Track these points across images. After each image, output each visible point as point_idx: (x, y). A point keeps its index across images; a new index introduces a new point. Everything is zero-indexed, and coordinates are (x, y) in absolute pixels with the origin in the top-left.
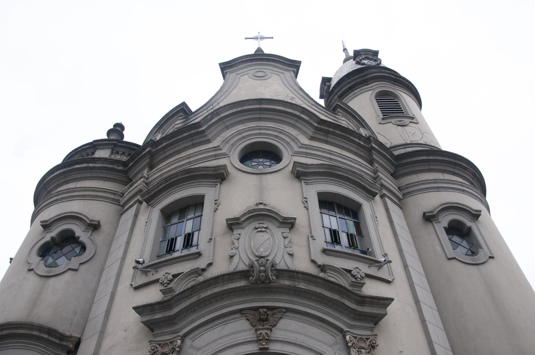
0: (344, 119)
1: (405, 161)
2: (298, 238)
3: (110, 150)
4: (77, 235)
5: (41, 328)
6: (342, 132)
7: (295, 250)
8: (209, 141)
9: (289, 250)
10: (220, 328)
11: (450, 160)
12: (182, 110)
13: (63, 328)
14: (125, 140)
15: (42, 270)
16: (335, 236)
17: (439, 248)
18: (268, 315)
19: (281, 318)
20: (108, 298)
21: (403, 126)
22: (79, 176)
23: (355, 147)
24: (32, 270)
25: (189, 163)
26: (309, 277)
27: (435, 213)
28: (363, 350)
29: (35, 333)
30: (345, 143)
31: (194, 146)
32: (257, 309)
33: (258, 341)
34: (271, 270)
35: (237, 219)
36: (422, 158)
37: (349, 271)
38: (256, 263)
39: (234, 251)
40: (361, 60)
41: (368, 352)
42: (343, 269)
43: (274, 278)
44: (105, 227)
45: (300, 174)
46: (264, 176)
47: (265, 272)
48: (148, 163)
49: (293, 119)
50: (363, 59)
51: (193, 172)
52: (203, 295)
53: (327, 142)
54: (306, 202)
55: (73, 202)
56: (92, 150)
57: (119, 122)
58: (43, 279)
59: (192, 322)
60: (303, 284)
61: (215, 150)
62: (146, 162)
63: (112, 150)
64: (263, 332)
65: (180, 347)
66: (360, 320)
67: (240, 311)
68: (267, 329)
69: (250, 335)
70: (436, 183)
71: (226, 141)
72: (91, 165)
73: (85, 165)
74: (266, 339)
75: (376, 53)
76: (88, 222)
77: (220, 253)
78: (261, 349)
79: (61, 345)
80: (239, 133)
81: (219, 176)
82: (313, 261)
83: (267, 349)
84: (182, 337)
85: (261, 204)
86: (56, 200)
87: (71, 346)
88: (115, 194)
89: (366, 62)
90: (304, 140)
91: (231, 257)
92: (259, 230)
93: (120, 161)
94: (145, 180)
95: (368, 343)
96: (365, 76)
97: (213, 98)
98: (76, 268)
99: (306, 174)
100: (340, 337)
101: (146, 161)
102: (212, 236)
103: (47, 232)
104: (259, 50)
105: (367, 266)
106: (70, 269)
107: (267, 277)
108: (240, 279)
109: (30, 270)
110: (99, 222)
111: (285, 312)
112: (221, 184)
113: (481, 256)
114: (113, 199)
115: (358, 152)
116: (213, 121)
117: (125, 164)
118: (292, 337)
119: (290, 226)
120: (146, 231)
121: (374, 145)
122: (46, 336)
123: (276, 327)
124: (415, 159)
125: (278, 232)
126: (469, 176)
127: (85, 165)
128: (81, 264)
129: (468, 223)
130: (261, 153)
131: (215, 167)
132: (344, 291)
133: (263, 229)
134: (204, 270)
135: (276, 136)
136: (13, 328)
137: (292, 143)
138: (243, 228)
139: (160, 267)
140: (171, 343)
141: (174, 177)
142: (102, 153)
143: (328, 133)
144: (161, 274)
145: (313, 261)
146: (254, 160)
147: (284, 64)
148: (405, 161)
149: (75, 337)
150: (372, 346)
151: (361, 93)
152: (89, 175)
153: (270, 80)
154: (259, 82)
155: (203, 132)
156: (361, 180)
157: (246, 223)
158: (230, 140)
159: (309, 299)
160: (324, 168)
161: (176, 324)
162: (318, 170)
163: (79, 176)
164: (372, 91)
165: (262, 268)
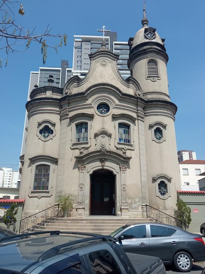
3: (51, 91)
4: (50, 127)
7: (111, 143)
9: (110, 143)
17: (151, 136)
27: (152, 125)
33: (102, 166)
37: (123, 148)
42: (121, 148)
45: (115, 117)
46: (104, 117)
64: (103, 164)
67: (98, 159)
76: (52, 123)
77: (94, 145)
80: (97, 98)
82: (115, 146)
85: (103, 128)
90: (117, 102)
91: (96, 145)
92: (103, 137)
99: (115, 118)
113: (162, 140)
121: (139, 100)
129: (162, 128)
130: (104, 107)
137: (113, 103)
145: (115, 146)
151: (143, 59)
155: (86, 96)
164: (147, 59)
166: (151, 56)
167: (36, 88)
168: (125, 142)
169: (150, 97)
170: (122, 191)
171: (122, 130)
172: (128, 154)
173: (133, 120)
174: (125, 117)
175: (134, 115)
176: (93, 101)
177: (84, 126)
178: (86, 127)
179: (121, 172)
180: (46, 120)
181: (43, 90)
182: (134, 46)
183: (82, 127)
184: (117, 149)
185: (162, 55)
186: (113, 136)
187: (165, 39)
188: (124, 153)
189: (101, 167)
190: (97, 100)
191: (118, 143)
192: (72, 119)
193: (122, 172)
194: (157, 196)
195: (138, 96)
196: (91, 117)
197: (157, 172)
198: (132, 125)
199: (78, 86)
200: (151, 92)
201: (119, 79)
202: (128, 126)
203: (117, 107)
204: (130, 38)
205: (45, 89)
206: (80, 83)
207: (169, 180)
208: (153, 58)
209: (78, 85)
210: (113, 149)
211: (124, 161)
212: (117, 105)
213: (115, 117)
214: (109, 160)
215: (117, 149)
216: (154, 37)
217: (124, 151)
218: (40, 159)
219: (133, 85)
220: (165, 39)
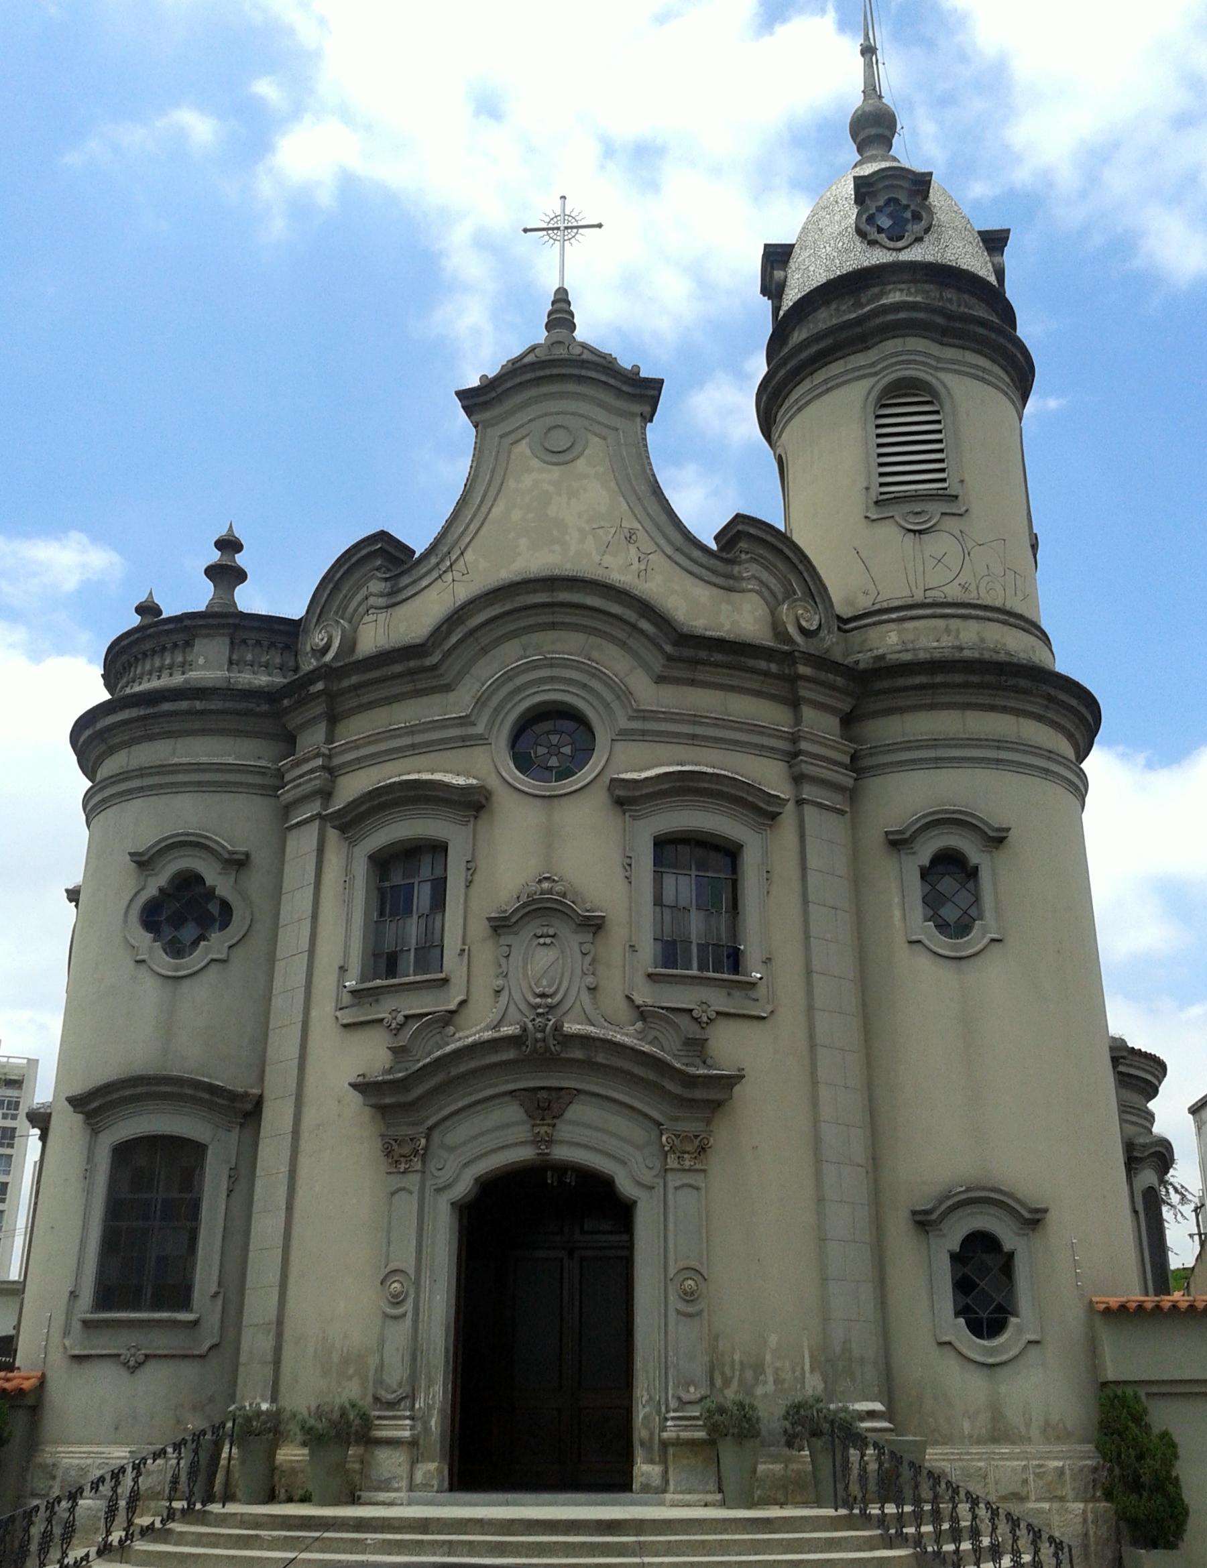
3: (227, 641)
20: (297, 1030)
24: (143, 961)
28: (686, 1156)
29: (189, 1091)
35: (505, 919)
38: (530, 1025)
39: (500, 982)
43: (558, 1048)
46: (556, 801)
47: (544, 1040)
54: (630, 865)
55: (180, 796)
58: (170, 981)
64: (543, 1130)
65: (426, 1148)
68: (549, 1125)
69: (522, 1132)
70: (935, 747)
77: (485, 993)
78: (539, 1154)
83: (547, 1154)
90: (647, 693)
91: (498, 992)
92: (542, 941)
98: (223, 956)
100: (656, 1132)
102: (464, 943)
103: (147, 876)
107: (547, 1049)
110: (247, 855)
112: (476, 818)
113: (976, 939)
114: (262, 786)
116: (454, 639)
120: (348, 903)
125: (573, 940)
128: (230, 947)
130: (550, 736)
133: (548, 940)
138: (516, 933)
140: (412, 1140)
143: (695, 663)
144: (382, 1011)
149: (254, 1095)
155: (434, 668)
164: (873, 380)
165: (539, 1035)
166: (903, 362)
167: (149, 620)
168: (700, 969)
169: (889, 641)
170: (672, 1314)
171: (680, 887)
173: (764, 811)
174: (164, 1097)
175: (770, 776)
176: (481, 702)
177: (426, 860)
178: (438, 873)
179: (671, 1185)
180: (188, 834)
181: (175, 637)
182: (792, 296)
183: (405, 882)
184: (642, 1014)
185: (983, 346)
186: (617, 934)
187: (1008, 231)
188: (697, 1047)
189: (524, 1154)
191: (650, 976)
192: (351, 821)
193: (674, 1180)
194: (946, 1339)
195: (799, 639)
196: (473, 804)
197: (937, 1157)
199: (394, 599)
200: (896, 603)
202: (731, 853)
203: (646, 728)
204: (766, 246)
205: (189, 628)
206: (405, 580)
207: (1034, 1221)
208: (907, 373)
209: (389, 594)
211: (693, 1098)
212: (643, 715)
213: (628, 799)
214: (582, 1097)
215: (642, 1014)
216: (918, 228)
217: (692, 1030)
219: (766, 568)
220: (1008, 231)
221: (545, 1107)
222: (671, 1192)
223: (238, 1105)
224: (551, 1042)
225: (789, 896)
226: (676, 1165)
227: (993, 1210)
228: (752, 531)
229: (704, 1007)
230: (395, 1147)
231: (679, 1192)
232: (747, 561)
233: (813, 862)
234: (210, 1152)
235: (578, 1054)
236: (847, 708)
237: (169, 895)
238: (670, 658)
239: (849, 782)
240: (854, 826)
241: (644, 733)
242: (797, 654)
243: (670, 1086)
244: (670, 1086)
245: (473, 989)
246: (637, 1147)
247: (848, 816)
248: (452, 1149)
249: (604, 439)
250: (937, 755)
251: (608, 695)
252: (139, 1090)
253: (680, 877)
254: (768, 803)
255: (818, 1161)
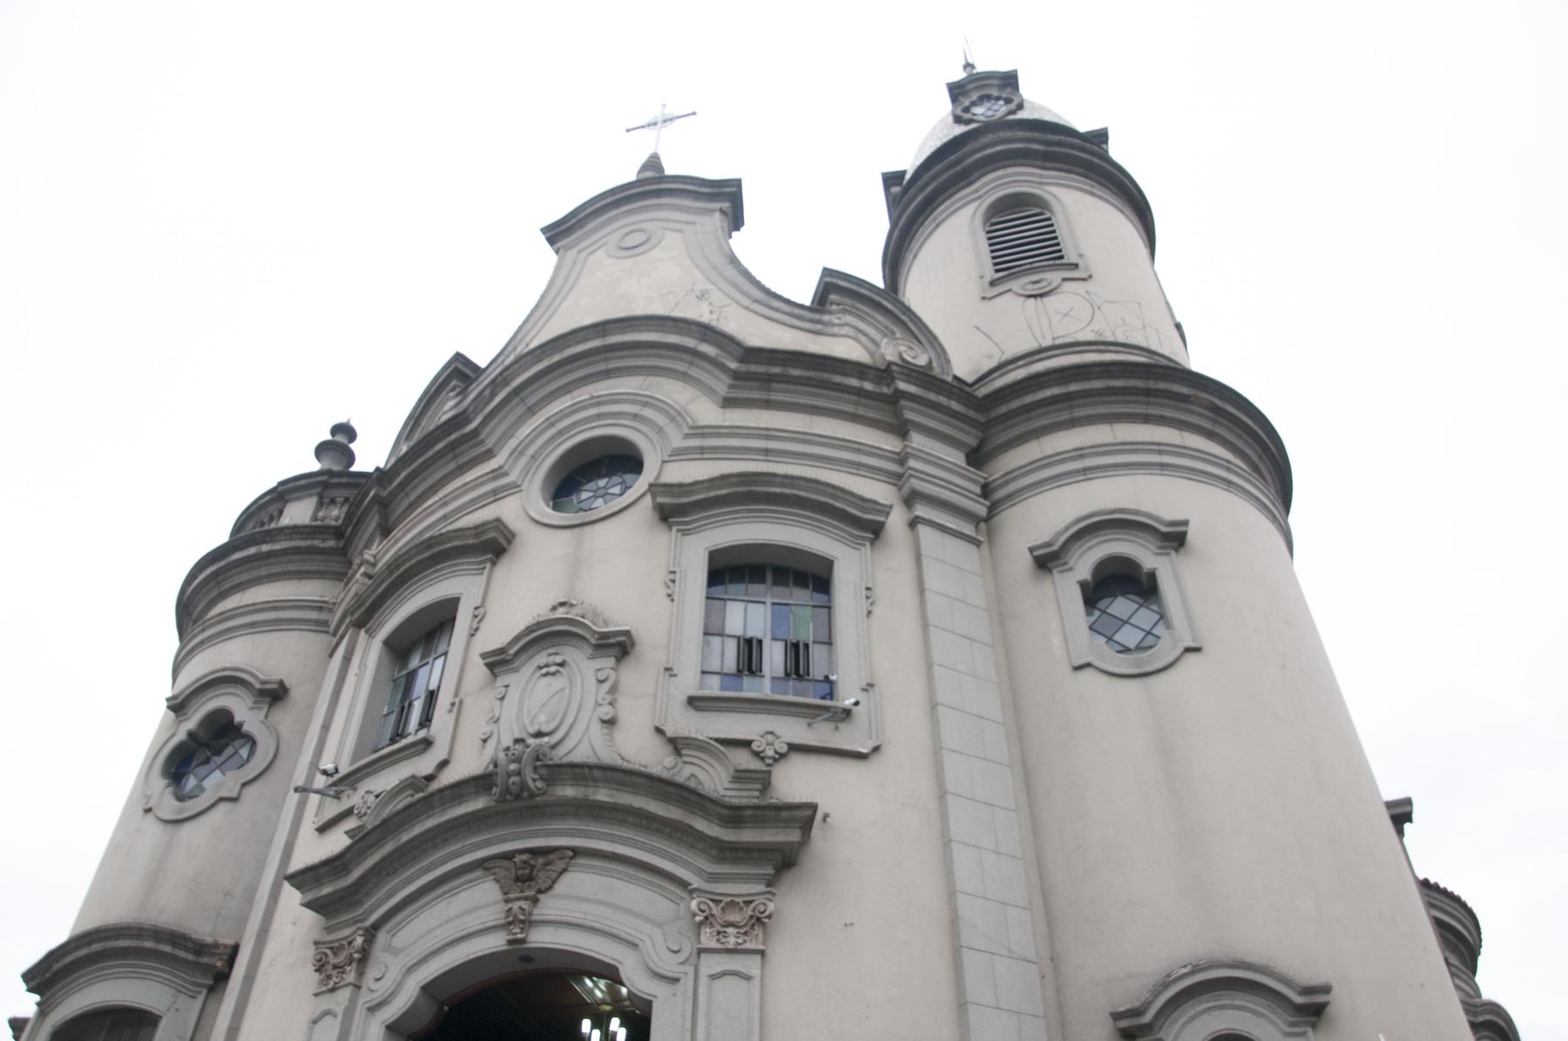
0: (848, 318)
1: (1003, 409)
2: (637, 678)
3: (315, 500)
4: (237, 719)
5: (157, 934)
6: (808, 369)
8: (489, 454)
10: (443, 904)
11: (1131, 383)
12: (459, 371)
13: (203, 930)
14: (357, 467)
15: (170, 807)
16: (750, 650)
18: (532, 867)
19: (565, 870)
21: (1041, 295)
22: (244, 577)
23: (850, 402)
25: (445, 517)
26: (616, 775)
27: (1056, 547)
28: (730, 930)
29: (149, 944)
30: (817, 395)
31: (462, 469)
32: (507, 856)
34: (535, 769)
35: (501, 651)
36: (1048, 393)
37: (746, 744)
39: (488, 728)
40: (966, 110)
41: (746, 933)
42: (717, 740)
43: (540, 784)
44: (297, 693)
45: (675, 509)
46: (588, 529)
47: (519, 773)
48: (379, 525)
49: (683, 360)
50: (973, 104)
51: (439, 544)
52: (405, 837)
53: (768, 405)
56: (278, 505)
57: (343, 420)
58: (170, 827)
59: (390, 895)
60: (604, 791)
61: (495, 479)
62: (373, 525)
63: (321, 497)
66: (735, 861)
67: (481, 864)
68: (526, 899)
70: (1082, 457)
71: (518, 452)
72: (265, 548)
73: (252, 550)
74: (522, 922)
75: (1009, 80)
79: (199, 964)
81: (492, 545)
83: (523, 941)
84: (367, 930)
86: (202, 642)
87: (219, 964)
88: (320, 609)
89: (979, 110)
90: (707, 412)
92: (544, 671)
93: (327, 527)
94: (371, 571)
95: (749, 911)
96: (958, 162)
97: (520, 328)
98: (234, 794)
101: (372, 523)
102: (456, 695)
104: (653, 163)
105: (803, 722)
106: (221, 799)
107: (523, 786)
108: (477, 794)
109: (148, 811)
111: (571, 858)
112: (494, 564)
113: (1165, 651)
115: (861, 411)
117: (338, 532)
118: (575, 911)
119: (615, 651)
121: (902, 386)
122: (168, 949)
123: (552, 892)
124: (1029, 399)
125: (585, 667)
126: (1200, 415)
127: (252, 550)
128: (244, 785)
131: (476, 527)
132: (694, 798)
134: (430, 778)
135: (635, 416)
136: (108, 938)
138: (516, 670)
139: (360, 779)
141: (405, 562)
142: (299, 513)
143: (767, 380)
145: (659, 731)
146: (587, 487)
147: (697, 196)
148: (1003, 409)
149: (225, 946)
150: (759, 919)
152: (263, 572)
153: (655, 253)
154: (628, 263)
156: (835, 497)
157: (524, 657)
158: (527, 446)
159: (623, 823)
160: (730, 485)
161: (360, 903)
162: (712, 494)
163: (244, 577)
164: (976, 204)
171: (749, 615)
172: (797, 782)
174: (125, 953)
179: (704, 972)
188: (764, 781)
190: (553, 431)
198: (850, 565)
201: (738, 296)
202: (814, 577)
210: (637, 746)
211: (754, 844)
212: (700, 431)
214: (581, 861)
215: (677, 745)
218: (125, 953)
221: (529, 875)
222: (703, 981)
223: (205, 960)
224: (529, 775)
225: (900, 615)
226: (713, 944)
227: (1241, 999)
228: (842, 283)
229: (770, 738)
230: (716, 910)
231: (719, 983)
232: (838, 312)
233: (932, 582)
234: (162, 1025)
235: (569, 792)
236: (973, 442)
237: (201, 745)
238: (737, 376)
239: (981, 510)
240: (995, 566)
241: (702, 450)
242: (894, 368)
243: (701, 825)
244: (701, 825)
245: (458, 748)
246: (659, 925)
247: (985, 547)
248: (395, 952)
249: (681, 231)
250: (1085, 468)
251: (660, 419)
252: (96, 947)
253: (750, 606)
254: (865, 510)
255: (957, 951)
